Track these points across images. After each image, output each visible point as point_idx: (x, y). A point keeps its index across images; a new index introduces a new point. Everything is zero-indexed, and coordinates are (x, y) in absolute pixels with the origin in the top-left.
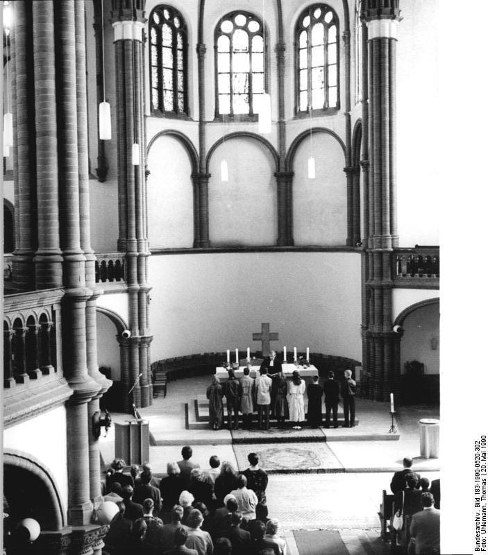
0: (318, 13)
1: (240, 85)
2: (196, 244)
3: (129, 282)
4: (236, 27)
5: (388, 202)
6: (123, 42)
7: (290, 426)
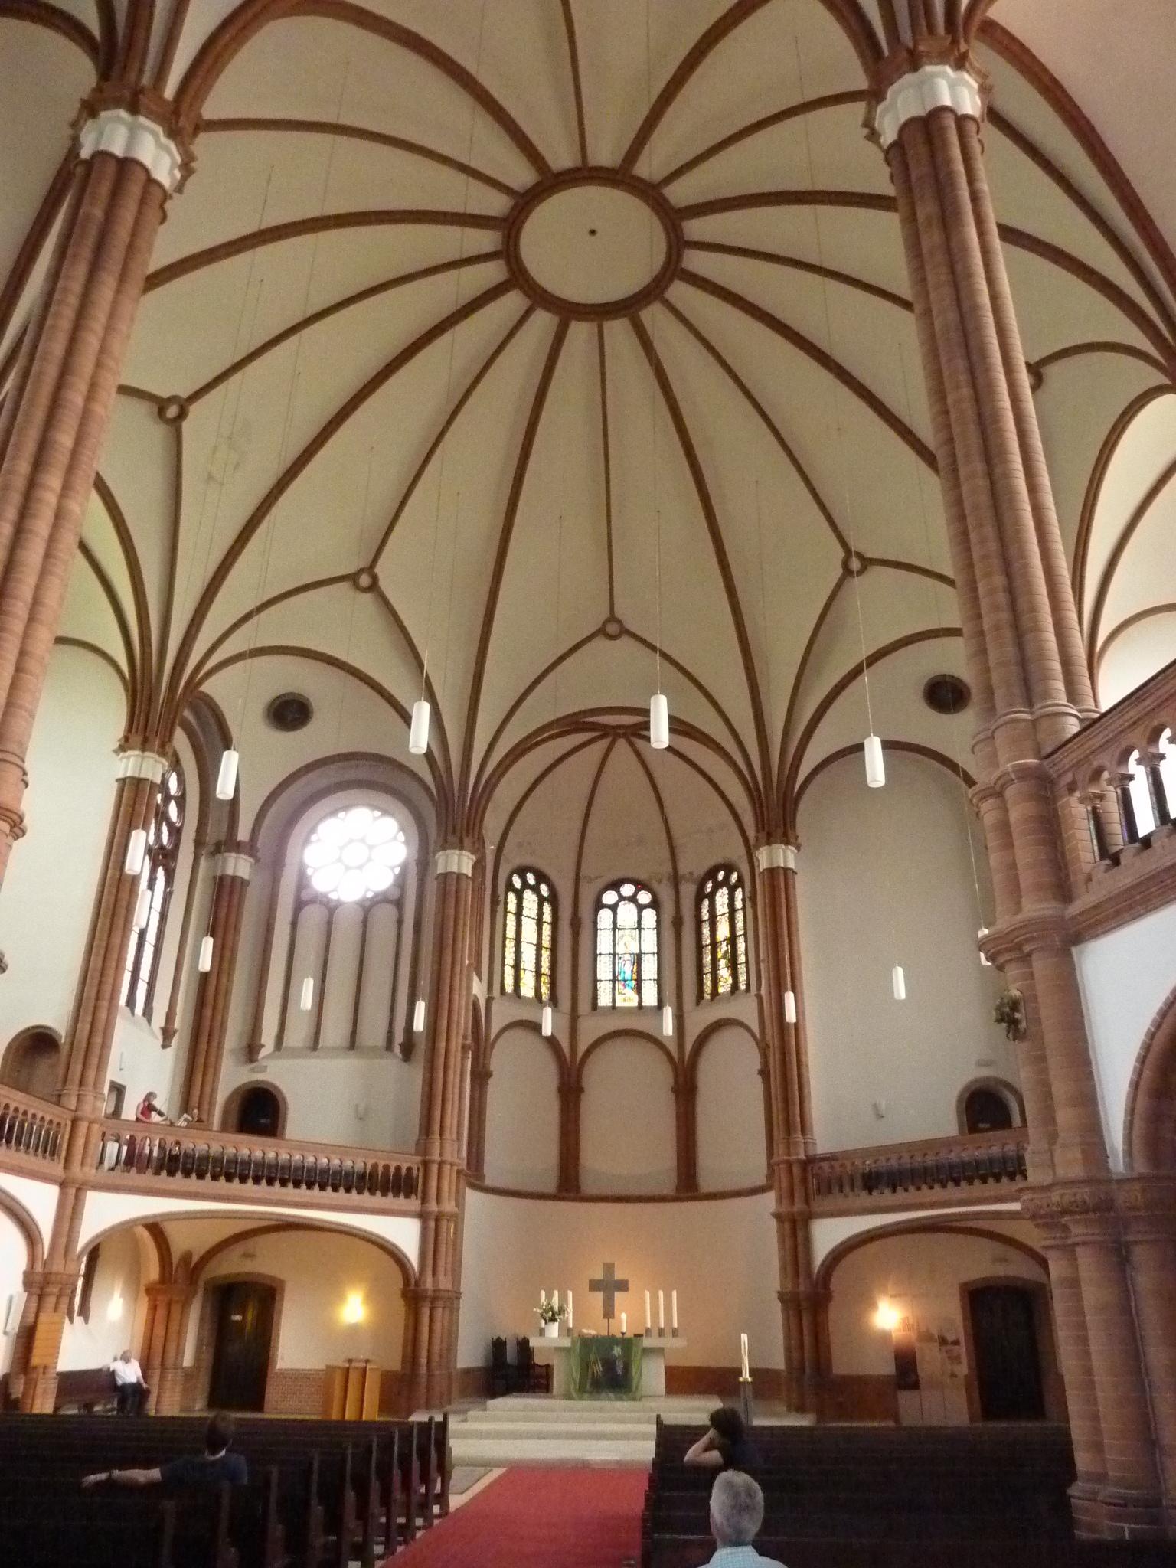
0: (721, 875)
1: (627, 969)
3: (424, 1200)
4: (622, 898)
5: (796, 1087)
6: (445, 876)
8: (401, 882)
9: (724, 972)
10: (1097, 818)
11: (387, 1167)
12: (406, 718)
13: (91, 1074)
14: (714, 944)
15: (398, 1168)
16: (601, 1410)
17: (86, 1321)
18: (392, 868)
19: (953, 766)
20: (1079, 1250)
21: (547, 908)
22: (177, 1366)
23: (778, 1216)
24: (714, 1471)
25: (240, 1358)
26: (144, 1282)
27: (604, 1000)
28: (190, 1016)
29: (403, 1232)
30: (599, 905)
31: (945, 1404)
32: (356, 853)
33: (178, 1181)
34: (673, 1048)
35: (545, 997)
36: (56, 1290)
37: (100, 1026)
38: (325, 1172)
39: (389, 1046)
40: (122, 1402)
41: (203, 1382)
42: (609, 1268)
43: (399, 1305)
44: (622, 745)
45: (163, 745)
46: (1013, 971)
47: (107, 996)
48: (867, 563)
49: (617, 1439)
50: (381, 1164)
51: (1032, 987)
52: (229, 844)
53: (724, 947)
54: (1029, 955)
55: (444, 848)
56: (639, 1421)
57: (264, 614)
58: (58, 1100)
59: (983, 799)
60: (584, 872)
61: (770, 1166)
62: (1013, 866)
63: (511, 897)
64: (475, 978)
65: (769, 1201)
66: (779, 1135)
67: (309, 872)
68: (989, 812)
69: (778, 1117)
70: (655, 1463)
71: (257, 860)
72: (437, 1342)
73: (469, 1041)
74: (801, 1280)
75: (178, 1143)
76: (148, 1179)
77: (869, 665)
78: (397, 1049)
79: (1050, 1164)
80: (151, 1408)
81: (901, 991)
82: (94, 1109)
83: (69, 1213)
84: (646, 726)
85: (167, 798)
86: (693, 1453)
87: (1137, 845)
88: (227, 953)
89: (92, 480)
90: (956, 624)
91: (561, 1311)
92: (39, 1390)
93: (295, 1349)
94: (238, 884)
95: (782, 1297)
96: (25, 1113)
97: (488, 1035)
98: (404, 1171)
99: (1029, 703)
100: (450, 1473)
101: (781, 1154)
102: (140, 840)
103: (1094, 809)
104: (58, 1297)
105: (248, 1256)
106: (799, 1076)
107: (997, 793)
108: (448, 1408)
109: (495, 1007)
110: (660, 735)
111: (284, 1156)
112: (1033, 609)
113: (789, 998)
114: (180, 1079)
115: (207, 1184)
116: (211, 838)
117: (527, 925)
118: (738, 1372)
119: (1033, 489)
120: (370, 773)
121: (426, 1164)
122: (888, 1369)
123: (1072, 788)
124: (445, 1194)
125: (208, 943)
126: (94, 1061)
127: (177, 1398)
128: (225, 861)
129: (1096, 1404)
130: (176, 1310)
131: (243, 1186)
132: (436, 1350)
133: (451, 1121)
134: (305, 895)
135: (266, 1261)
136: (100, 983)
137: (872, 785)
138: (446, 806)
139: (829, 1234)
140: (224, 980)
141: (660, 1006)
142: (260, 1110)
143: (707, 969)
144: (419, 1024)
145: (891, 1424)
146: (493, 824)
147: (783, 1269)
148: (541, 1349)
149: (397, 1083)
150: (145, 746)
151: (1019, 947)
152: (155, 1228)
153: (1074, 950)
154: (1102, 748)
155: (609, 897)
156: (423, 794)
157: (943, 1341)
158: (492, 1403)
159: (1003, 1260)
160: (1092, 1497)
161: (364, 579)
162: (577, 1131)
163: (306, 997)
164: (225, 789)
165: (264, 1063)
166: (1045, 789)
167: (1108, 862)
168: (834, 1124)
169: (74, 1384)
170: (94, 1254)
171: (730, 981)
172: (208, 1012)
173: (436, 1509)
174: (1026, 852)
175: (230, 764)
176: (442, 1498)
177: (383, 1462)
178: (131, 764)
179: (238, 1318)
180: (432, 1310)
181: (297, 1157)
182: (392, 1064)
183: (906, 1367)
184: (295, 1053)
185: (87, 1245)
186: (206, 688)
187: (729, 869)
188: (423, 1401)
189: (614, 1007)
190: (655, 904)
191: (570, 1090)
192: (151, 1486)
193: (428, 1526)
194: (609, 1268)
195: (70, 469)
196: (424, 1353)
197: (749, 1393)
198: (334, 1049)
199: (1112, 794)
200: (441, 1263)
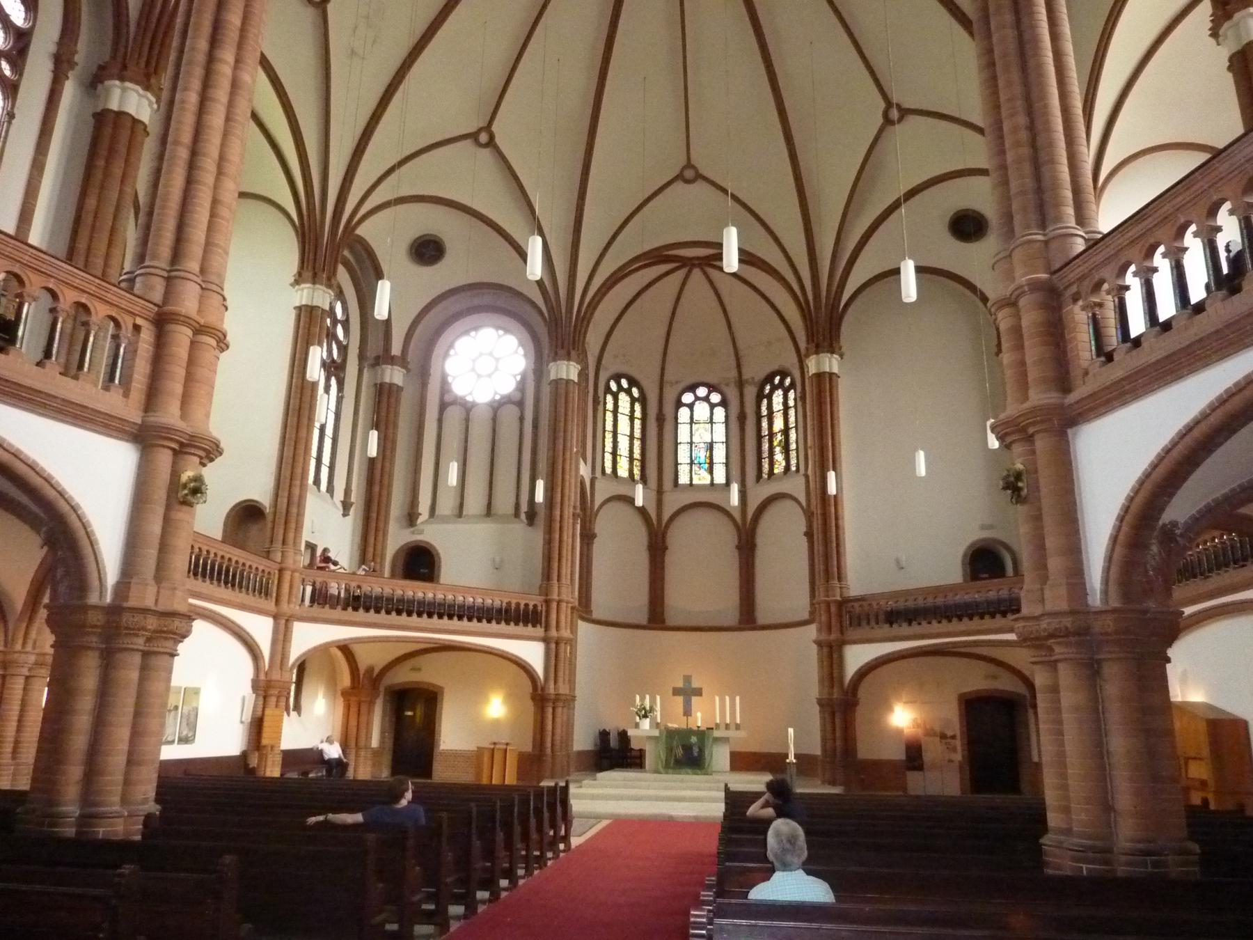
1: (702, 455)
2: (650, 620)
3: (547, 628)
4: (697, 398)
6: (557, 382)
7: (95, 82)
8: (521, 387)
9: (779, 457)
10: (1096, 324)
11: (518, 605)
12: (523, 255)
13: (291, 535)
14: (771, 435)
15: (526, 605)
16: (682, 781)
17: (299, 714)
18: (515, 376)
19: (972, 287)
20: (1061, 666)
21: (637, 407)
22: (367, 747)
23: (819, 644)
24: (767, 822)
25: (413, 744)
26: (339, 688)
27: (684, 479)
28: (363, 490)
29: (532, 652)
30: (679, 404)
31: (944, 780)
32: (486, 364)
33: (361, 615)
34: (737, 516)
35: (637, 477)
36: (276, 692)
37: (296, 499)
38: (471, 608)
39: (517, 514)
40: (329, 772)
41: (387, 759)
42: (687, 679)
43: (530, 706)
44: (697, 273)
45: (329, 279)
46: (1018, 449)
47: (299, 476)
48: (905, 112)
49: (697, 801)
50: (514, 602)
51: (1035, 463)
52: (385, 358)
53: (779, 437)
54: (1032, 436)
55: (555, 360)
56: (710, 789)
57: (404, 168)
58: (267, 555)
59: (1000, 308)
60: (666, 378)
61: (812, 604)
62: (1022, 363)
63: (609, 398)
64: (582, 462)
65: (812, 631)
66: (820, 582)
67: (450, 379)
68: (1004, 320)
69: (820, 567)
70: (725, 816)
71: (408, 371)
72: (558, 731)
73: (578, 511)
74: (835, 690)
75: (359, 587)
76: (338, 613)
77: (905, 201)
78: (523, 516)
79: (1042, 600)
80: (350, 774)
81: (922, 470)
82: (295, 561)
83: (282, 638)
84: (719, 257)
85: (335, 321)
86: (754, 810)
87: (1129, 345)
88: (389, 445)
89: (249, 115)
90: (983, 164)
91: (652, 709)
92: (269, 763)
93: (453, 735)
94: (395, 389)
95: (820, 703)
96: (244, 565)
97: (592, 508)
98: (531, 607)
99: (1043, 225)
100: (571, 822)
101: (821, 596)
102: (317, 355)
103: (1094, 315)
104: (278, 697)
105: (416, 669)
106: (837, 535)
107: (1011, 303)
108: (569, 778)
109: (598, 485)
110: (731, 261)
111: (440, 596)
112: (1051, 144)
113: (831, 476)
114: (358, 539)
115: (382, 617)
116: (371, 354)
117: (622, 421)
118: (786, 756)
119: (1055, 37)
120: (492, 298)
121: (547, 602)
122: (899, 754)
123: (1075, 299)
124: (563, 624)
125: (374, 436)
126: (293, 525)
127: (369, 769)
128: (383, 371)
129: (1066, 779)
130: (364, 708)
131: (410, 619)
132: (558, 738)
133: (566, 570)
134: (447, 398)
135: (429, 673)
136: (293, 467)
137: (906, 300)
138: (557, 325)
139: (857, 656)
140: (387, 464)
141: (728, 484)
142: (420, 562)
143: (766, 454)
144: (540, 497)
145: (900, 793)
146: (593, 339)
147: (821, 681)
148: (636, 737)
149: (524, 542)
150: (315, 280)
151: (1023, 430)
152: (345, 648)
153: (1070, 431)
154: (1104, 264)
155: (688, 398)
156: (539, 318)
157: (943, 736)
158: (600, 775)
159: (995, 677)
160: (1059, 846)
161: (483, 138)
162: (662, 579)
163: (452, 476)
164: (381, 310)
165: (421, 527)
166: (1052, 298)
167: (1103, 359)
168: (864, 572)
169: (292, 758)
170: (302, 668)
171: (784, 463)
172: (376, 489)
173: (562, 846)
174: (1034, 352)
175: (384, 293)
176: (566, 839)
177: (517, 815)
178: (306, 295)
179: (410, 713)
180: (554, 709)
181: (450, 597)
182: (519, 528)
183: (914, 754)
184: (445, 520)
185: (297, 660)
186: (359, 231)
187: (784, 374)
188: (547, 774)
189: (691, 484)
190: (724, 403)
191: (657, 548)
192: (355, 826)
193: (556, 857)
194: (687, 679)
195: (240, 46)
196: (549, 739)
197: (794, 770)
198: (475, 516)
199: (1110, 302)
200: (561, 674)
